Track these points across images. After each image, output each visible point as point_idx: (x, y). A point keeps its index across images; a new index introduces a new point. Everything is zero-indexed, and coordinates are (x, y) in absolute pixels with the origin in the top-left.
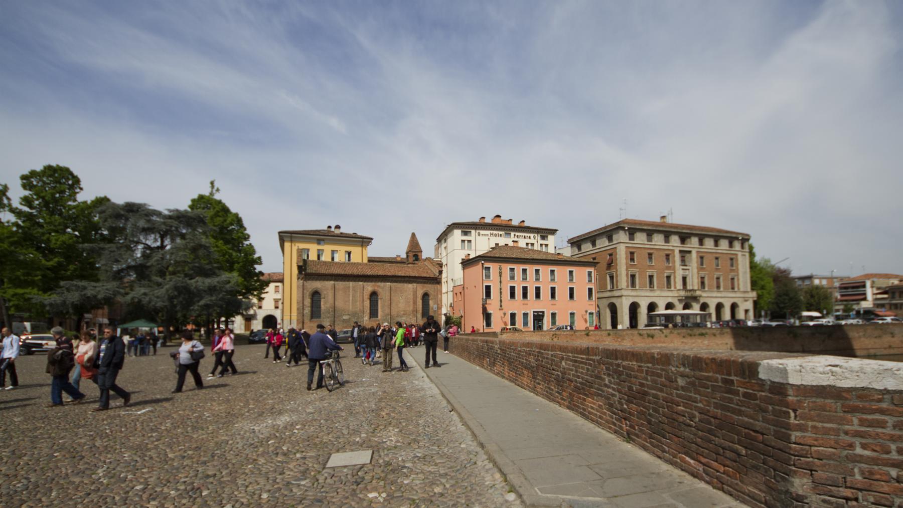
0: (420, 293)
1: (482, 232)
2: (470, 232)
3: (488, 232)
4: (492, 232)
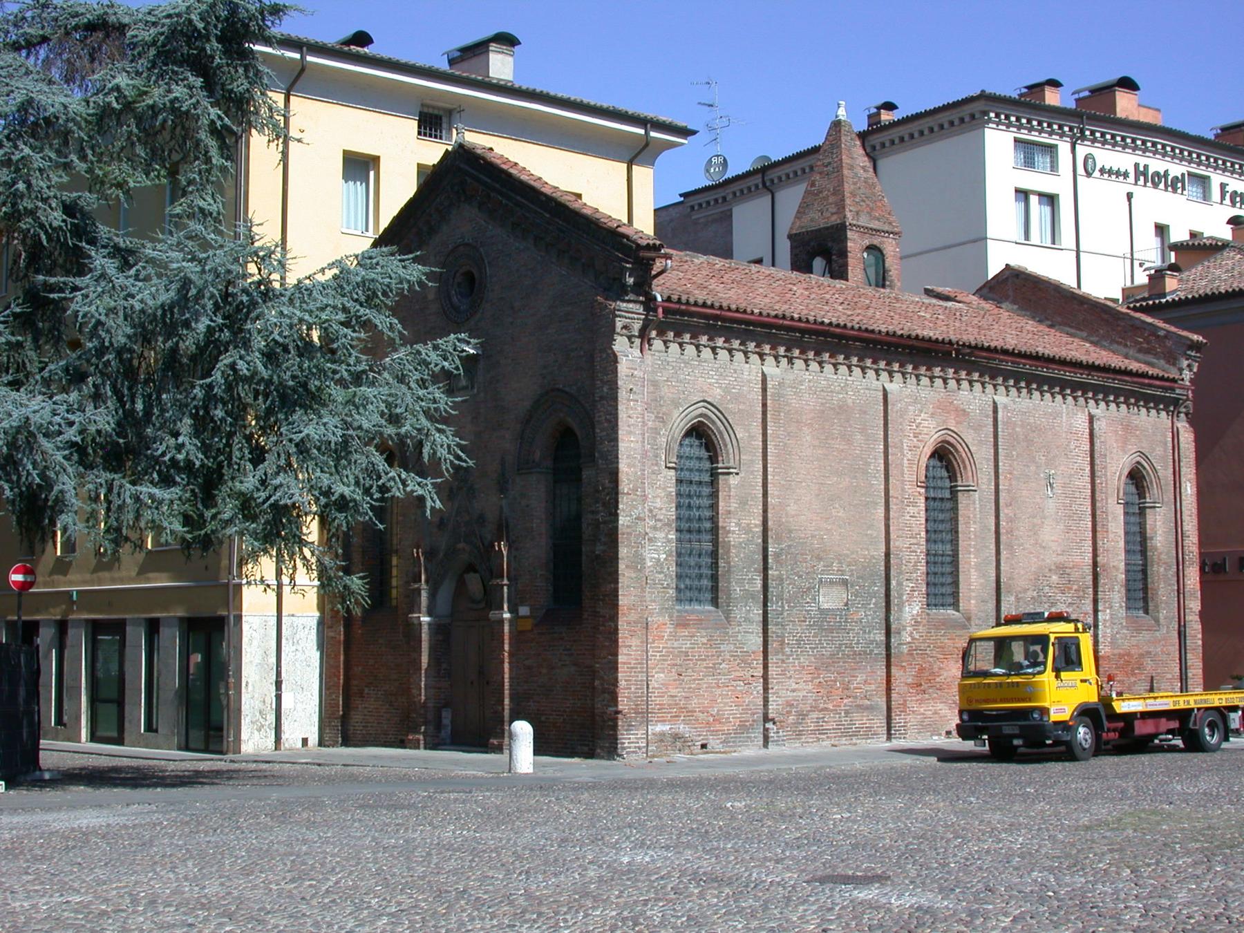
0: (1117, 466)
1: (1107, 157)
2: (1051, 149)
3: (1124, 160)
4: (1142, 161)
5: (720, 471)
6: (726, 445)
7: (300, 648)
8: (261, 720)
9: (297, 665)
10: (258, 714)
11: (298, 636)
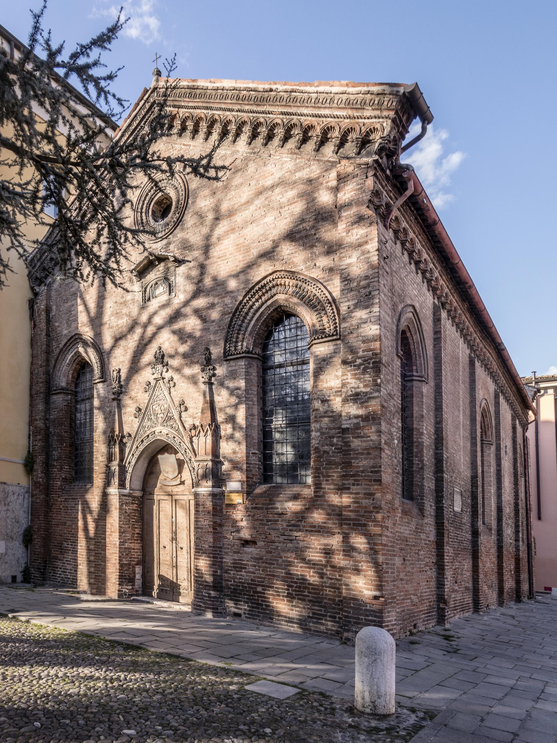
6: (420, 357)
7: (10, 508)
9: (8, 521)
11: (9, 500)
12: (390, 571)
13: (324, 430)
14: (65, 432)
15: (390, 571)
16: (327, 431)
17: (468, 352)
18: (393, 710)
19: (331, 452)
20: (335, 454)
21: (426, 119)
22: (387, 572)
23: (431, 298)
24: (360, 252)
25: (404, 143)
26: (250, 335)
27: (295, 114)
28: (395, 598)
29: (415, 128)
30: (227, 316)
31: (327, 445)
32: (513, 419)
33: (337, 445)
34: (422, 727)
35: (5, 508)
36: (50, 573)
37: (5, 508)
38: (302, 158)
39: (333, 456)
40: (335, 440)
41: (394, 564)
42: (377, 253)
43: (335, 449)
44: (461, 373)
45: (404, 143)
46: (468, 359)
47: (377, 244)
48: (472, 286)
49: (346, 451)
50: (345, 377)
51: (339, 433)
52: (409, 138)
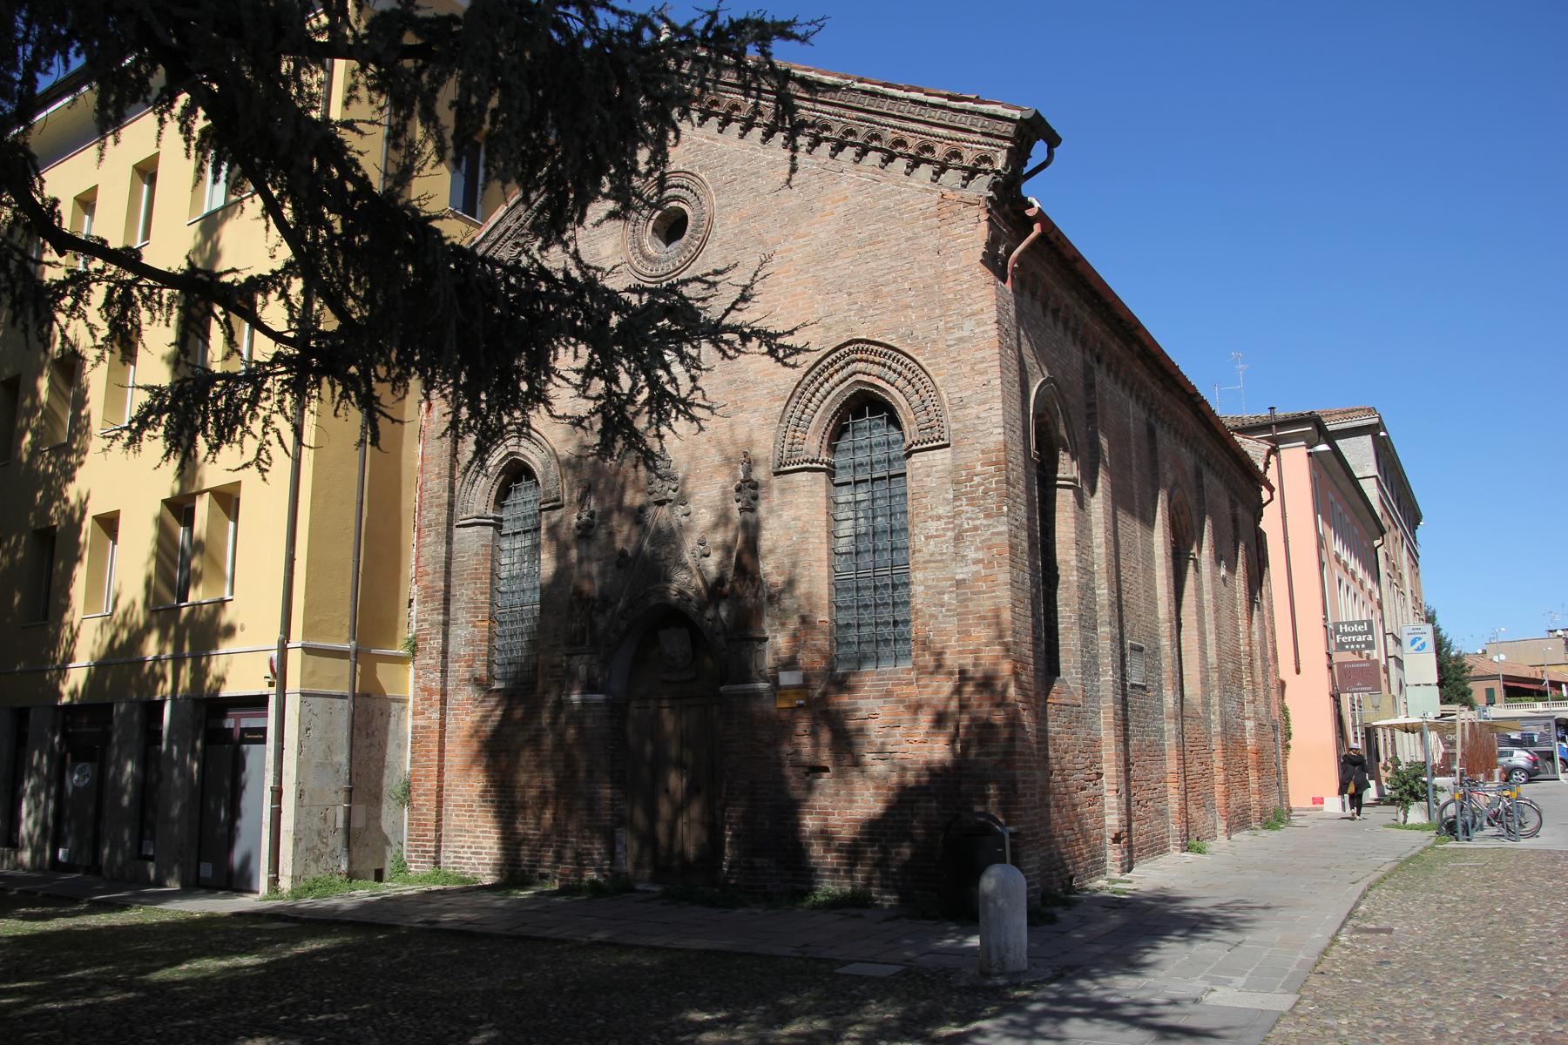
5: (1059, 482)
8: (320, 846)
10: (316, 838)
12: (1028, 792)
13: (930, 583)
14: (482, 593)
15: (1028, 792)
16: (935, 583)
17: (1144, 416)
18: (1025, 966)
19: (940, 616)
20: (948, 619)
21: (1053, 140)
22: (1025, 795)
23: (1079, 354)
24: (973, 323)
25: (1026, 170)
26: (814, 432)
27: (878, 124)
28: (1037, 834)
29: (1039, 151)
30: (777, 404)
31: (935, 605)
32: (1233, 505)
33: (950, 604)
34: (576, 251)
35: (367, 742)
36: (448, 858)
37: (367, 742)
38: (888, 180)
39: (944, 623)
40: (946, 597)
41: (1035, 781)
42: (996, 326)
43: (948, 610)
44: (1134, 455)
45: (1026, 170)
46: (1145, 429)
47: (995, 313)
48: (1139, 326)
49: (963, 614)
50: (958, 503)
51: (951, 586)
52: (1031, 164)
